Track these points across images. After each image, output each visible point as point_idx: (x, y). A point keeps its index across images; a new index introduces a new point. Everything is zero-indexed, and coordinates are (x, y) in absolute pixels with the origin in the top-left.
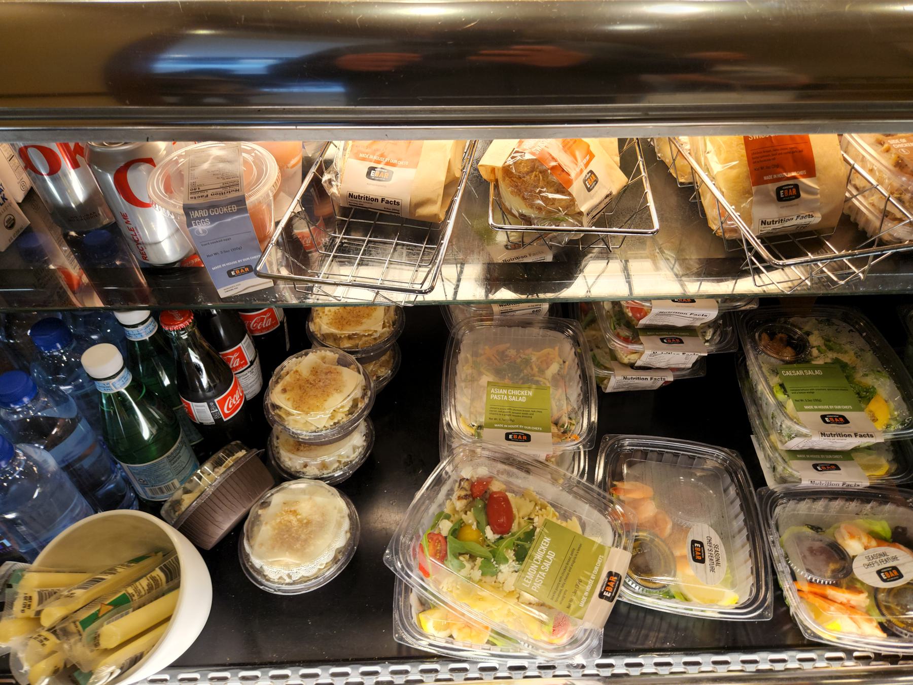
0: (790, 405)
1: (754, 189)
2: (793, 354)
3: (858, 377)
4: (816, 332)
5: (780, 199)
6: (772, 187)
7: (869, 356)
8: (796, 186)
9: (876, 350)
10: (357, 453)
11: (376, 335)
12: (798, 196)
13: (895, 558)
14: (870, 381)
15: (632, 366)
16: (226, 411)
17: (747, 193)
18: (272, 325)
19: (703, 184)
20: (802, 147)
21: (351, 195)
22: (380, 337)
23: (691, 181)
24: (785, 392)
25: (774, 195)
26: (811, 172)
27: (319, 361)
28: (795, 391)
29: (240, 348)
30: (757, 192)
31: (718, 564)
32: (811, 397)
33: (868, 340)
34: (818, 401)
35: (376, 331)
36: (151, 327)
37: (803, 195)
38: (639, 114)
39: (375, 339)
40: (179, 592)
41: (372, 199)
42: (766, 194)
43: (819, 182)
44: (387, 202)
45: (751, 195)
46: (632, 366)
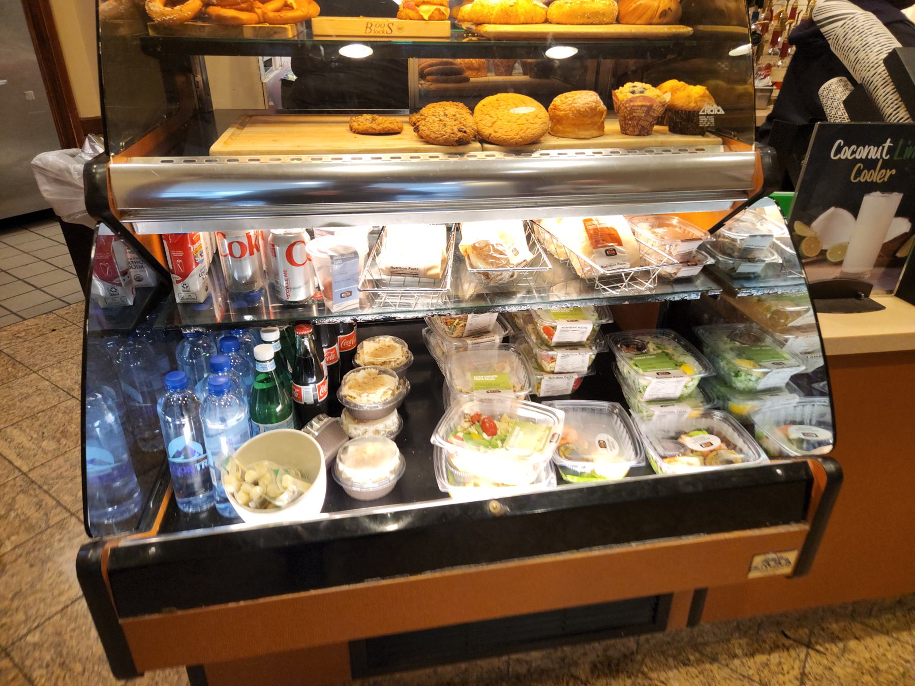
0: (641, 371)
1: (594, 250)
2: (782, 651)
3: (675, 357)
4: (651, 342)
5: (607, 255)
6: (603, 250)
7: (681, 349)
8: (614, 250)
9: (683, 346)
10: (395, 427)
11: (399, 362)
12: (616, 254)
13: (709, 438)
14: (682, 359)
15: (553, 372)
16: (321, 395)
17: (592, 253)
18: (335, 359)
19: (572, 253)
20: (613, 232)
21: (392, 267)
22: (401, 363)
23: (566, 258)
24: (636, 366)
25: (604, 253)
26: (620, 244)
27: (367, 375)
28: (641, 365)
29: (335, 349)
30: (596, 252)
31: (614, 448)
32: (650, 366)
33: (678, 342)
34: (655, 368)
35: (398, 359)
36: (278, 346)
37: (618, 253)
38: (533, 204)
39: (398, 364)
40: (309, 487)
41: (404, 269)
42: (601, 253)
43: (625, 248)
44: (412, 269)
45: (593, 254)
46: (553, 372)
